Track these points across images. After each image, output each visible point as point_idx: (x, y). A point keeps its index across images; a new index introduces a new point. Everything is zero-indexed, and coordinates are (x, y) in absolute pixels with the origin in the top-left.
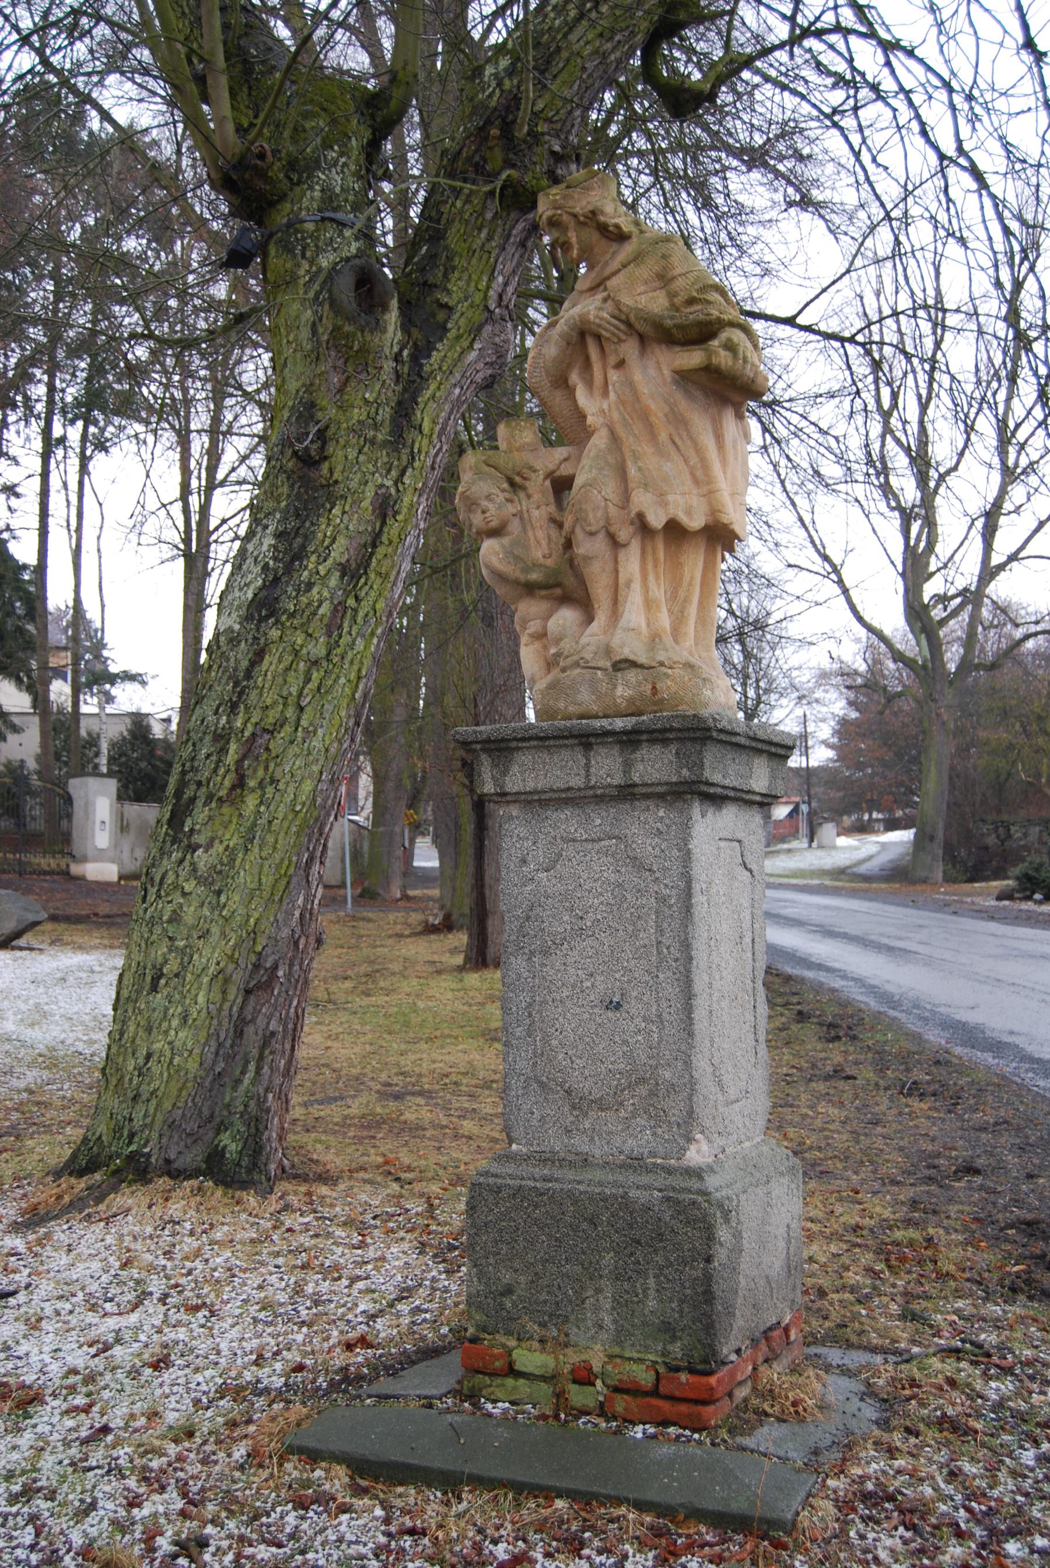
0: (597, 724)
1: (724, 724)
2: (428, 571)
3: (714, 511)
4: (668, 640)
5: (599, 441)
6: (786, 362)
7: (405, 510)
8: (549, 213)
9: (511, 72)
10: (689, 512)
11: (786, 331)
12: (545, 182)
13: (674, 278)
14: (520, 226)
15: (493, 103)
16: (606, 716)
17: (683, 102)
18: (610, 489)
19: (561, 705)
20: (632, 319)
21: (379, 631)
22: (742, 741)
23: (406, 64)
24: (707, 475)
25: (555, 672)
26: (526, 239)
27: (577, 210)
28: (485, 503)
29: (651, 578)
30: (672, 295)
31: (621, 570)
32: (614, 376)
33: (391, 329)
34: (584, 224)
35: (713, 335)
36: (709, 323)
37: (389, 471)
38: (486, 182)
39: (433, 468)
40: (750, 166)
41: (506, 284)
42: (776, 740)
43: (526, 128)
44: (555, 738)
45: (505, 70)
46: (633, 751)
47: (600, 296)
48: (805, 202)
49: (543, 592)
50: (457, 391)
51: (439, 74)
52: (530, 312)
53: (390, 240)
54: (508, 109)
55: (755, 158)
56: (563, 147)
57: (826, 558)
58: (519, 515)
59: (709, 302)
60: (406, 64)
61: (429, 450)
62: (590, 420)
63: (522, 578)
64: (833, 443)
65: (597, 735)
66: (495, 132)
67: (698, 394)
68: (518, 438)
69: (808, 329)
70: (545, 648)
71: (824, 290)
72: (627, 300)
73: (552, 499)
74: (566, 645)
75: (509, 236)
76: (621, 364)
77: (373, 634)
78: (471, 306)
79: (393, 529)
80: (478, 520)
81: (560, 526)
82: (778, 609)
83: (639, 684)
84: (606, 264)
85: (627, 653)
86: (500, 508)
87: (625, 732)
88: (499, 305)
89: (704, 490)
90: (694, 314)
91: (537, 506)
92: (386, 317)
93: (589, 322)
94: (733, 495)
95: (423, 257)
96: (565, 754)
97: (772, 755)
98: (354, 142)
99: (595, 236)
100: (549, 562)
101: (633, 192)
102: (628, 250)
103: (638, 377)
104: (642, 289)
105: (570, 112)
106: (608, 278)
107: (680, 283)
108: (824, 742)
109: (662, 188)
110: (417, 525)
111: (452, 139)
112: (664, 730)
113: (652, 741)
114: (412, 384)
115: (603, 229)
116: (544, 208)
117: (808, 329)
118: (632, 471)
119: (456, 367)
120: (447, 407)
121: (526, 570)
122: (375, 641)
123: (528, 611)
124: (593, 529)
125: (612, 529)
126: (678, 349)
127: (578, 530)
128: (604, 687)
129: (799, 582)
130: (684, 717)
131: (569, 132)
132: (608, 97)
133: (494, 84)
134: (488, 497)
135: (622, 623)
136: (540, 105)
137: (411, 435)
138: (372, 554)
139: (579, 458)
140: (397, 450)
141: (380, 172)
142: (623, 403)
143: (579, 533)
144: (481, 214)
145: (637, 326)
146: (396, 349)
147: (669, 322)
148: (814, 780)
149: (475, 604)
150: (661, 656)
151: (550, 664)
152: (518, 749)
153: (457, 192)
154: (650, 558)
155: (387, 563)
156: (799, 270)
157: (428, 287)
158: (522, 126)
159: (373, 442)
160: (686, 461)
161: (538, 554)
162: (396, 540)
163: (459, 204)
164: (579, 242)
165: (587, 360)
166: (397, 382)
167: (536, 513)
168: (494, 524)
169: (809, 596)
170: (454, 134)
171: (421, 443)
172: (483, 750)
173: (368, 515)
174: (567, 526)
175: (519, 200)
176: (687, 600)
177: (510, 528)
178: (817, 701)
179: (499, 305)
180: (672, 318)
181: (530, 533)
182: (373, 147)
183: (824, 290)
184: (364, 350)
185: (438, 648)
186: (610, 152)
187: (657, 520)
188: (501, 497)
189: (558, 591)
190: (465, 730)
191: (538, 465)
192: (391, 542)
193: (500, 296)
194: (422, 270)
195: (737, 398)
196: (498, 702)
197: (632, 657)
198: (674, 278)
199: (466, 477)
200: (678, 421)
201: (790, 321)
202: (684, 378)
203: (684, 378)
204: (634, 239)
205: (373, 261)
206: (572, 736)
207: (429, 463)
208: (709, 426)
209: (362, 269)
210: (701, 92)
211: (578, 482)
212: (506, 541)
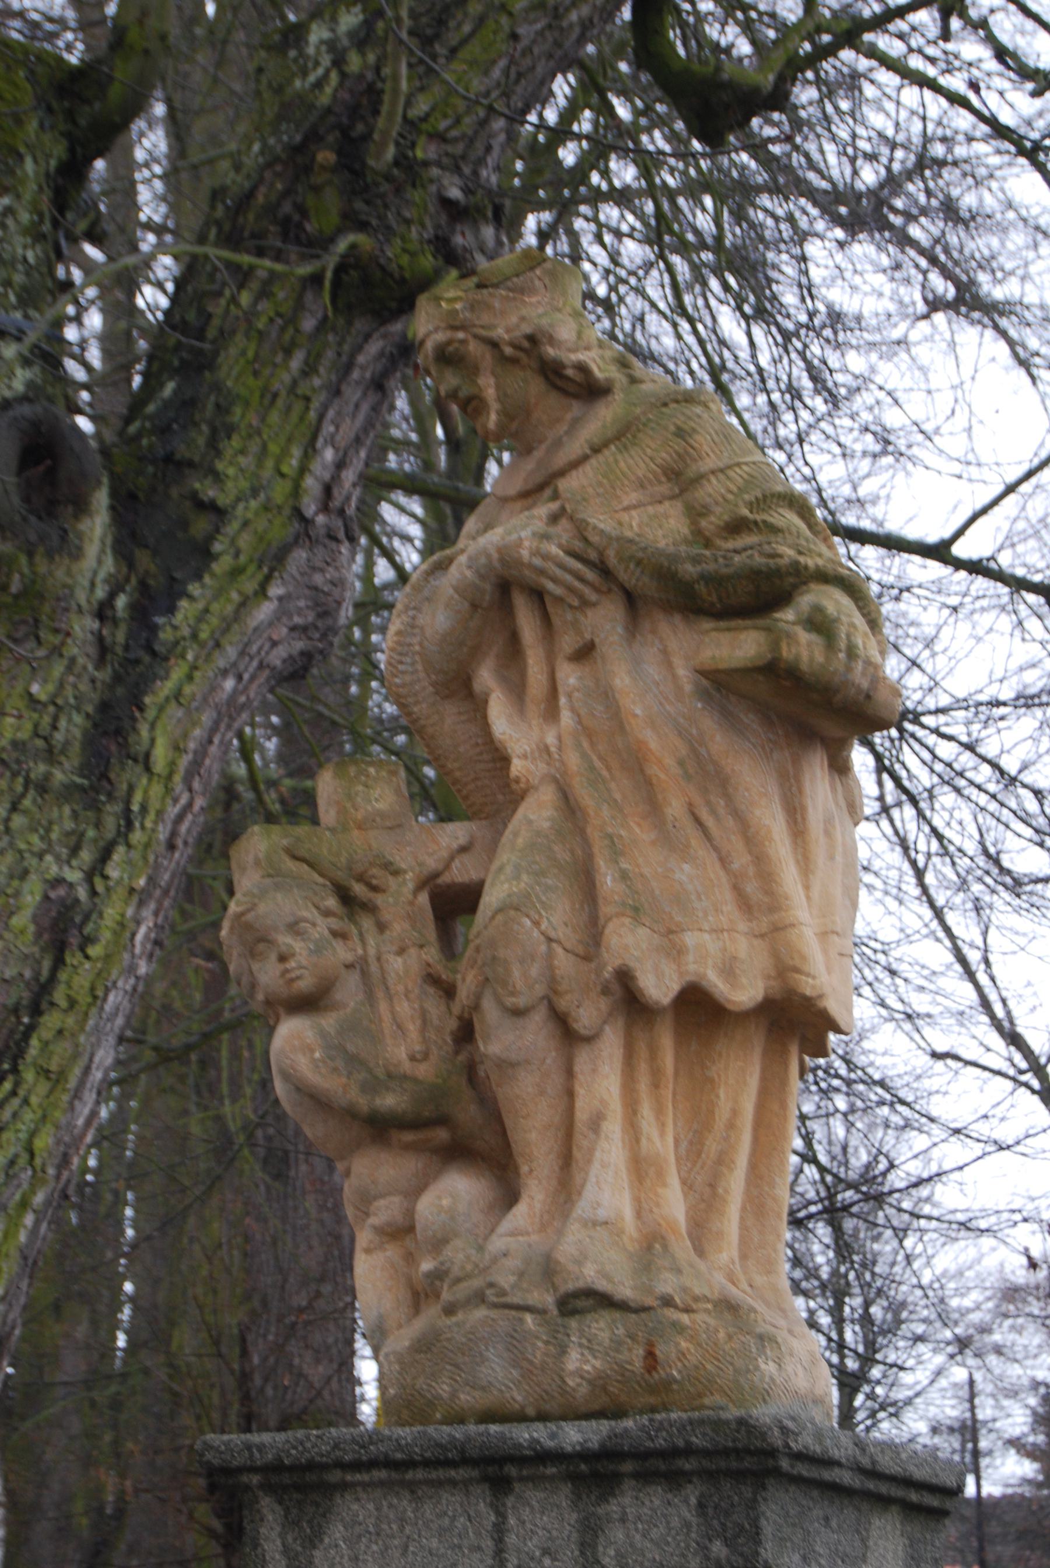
0: (524, 1434)
1: (806, 1441)
2: (149, 1055)
3: (785, 968)
4: (682, 1248)
5: (537, 812)
6: (930, 631)
7: (106, 935)
8: (440, 337)
9: (363, 38)
10: (729, 970)
11: (935, 569)
12: (428, 261)
13: (700, 478)
14: (374, 347)
15: (325, 98)
16: (542, 1417)
17: (716, 105)
18: (559, 917)
19: (444, 1389)
20: (612, 559)
21: (39, 1198)
22: (846, 1478)
23: (144, 14)
24: (769, 892)
25: (431, 1315)
26: (386, 374)
27: (500, 333)
28: (285, 940)
29: (646, 1110)
30: (695, 513)
31: (580, 1091)
32: (570, 676)
33: (92, 550)
34: (513, 361)
35: (782, 599)
36: (774, 574)
37: (75, 851)
38: (304, 258)
39: (171, 847)
40: (853, 226)
41: (340, 465)
42: (919, 1474)
43: (391, 152)
44: (427, 1464)
45: (351, 34)
46: (603, 1498)
47: (543, 510)
48: (967, 301)
49: (409, 1137)
50: (229, 684)
51: (211, 27)
52: (387, 511)
53: (94, 355)
54: (354, 111)
55: (862, 214)
56: (467, 191)
57: (1014, 1039)
58: (359, 966)
59: (774, 530)
60: (144, 14)
61: (166, 806)
62: (517, 766)
63: (364, 1104)
64: (1031, 805)
65: (521, 1460)
66: (326, 156)
67: (750, 719)
68: (361, 802)
69: (975, 568)
70: (410, 1258)
71: (1010, 489)
72: (601, 521)
73: (431, 933)
74: (458, 1254)
75: (349, 366)
76: (585, 653)
77: (24, 1204)
78: (266, 508)
79: (78, 975)
80: (268, 975)
81: (449, 991)
82: (910, 1156)
83: (617, 1344)
84: (558, 443)
85: (590, 1275)
86: (318, 950)
87: (584, 1455)
88: (325, 508)
89: (764, 924)
90: (743, 552)
91: (400, 947)
92: (84, 526)
93: (519, 563)
94: (824, 935)
95: (167, 404)
96: (450, 1501)
97: (911, 1510)
98: (29, 165)
99: (535, 387)
100: (424, 1071)
101: (611, 276)
102: (604, 416)
103: (622, 680)
104: (633, 497)
105: (483, 123)
106: (562, 473)
107: (712, 489)
108: (1015, 1443)
109: (670, 269)
110: (132, 969)
111: (237, 167)
112: (672, 1453)
113: (646, 1477)
114: (132, 665)
115: (552, 373)
116: (426, 324)
117: (975, 568)
118: (608, 880)
119: (228, 636)
120: (207, 718)
121: (372, 1086)
122: (29, 1219)
123: (374, 1175)
124: (521, 1001)
125: (563, 1004)
126: (707, 624)
127: (488, 1004)
128: (539, 1351)
129: (959, 1096)
130: (718, 1424)
131: (481, 162)
132: (562, 87)
133: (326, 60)
134: (294, 927)
135: (582, 1208)
136: (422, 106)
137: (125, 775)
138: (31, 1028)
139: (492, 848)
140: (96, 807)
141: (82, 226)
142: (589, 733)
143: (490, 1010)
144: (292, 320)
145: (623, 576)
146: (100, 593)
147: (689, 570)
148: (993, 1528)
149: (250, 1131)
150: (667, 1284)
151: (420, 1294)
152: (344, 1487)
153: (243, 276)
154: (643, 1068)
155: (62, 1049)
156: (956, 445)
157: (174, 465)
158: (383, 146)
159: (42, 788)
160: (724, 861)
161: (398, 1053)
162: (83, 999)
163: (245, 298)
164: (502, 396)
165: (514, 640)
166: (101, 662)
167: (396, 964)
168: (305, 984)
169: (982, 1129)
170: (243, 149)
171: (147, 792)
172: (268, 1488)
173: (27, 944)
174: (465, 992)
175: (379, 295)
176: (724, 1160)
177: (339, 995)
178: (998, 1350)
179: (325, 508)
180: (696, 560)
181: (383, 1006)
182: (71, 173)
183: (1010, 489)
184: (33, 594)
185: (165, 1225)
186: (568, 194)
187: (659, 986)
188: (322, 927)
189: (442, 1135)
190: (227, 1442)
191: (402, 859)
192: (72, 1003)
193: (328, 490)
194: (164, 431)
195: (831, 729)
196: (293, 1347)
197: (602, 1285)
198: (700, 478)
199: (247, 882)
200: (709, 776)
201: (939, 552)
202: (720, 685)
203: (720, 685)
204: (618, 396)
205: (60, 409)
206: (465, 1461)
207: (163, 834)
208: (773, 789)
209: (36, 425)
210: (756, 90)
211: (491, 898)
212: (329, 1022)
